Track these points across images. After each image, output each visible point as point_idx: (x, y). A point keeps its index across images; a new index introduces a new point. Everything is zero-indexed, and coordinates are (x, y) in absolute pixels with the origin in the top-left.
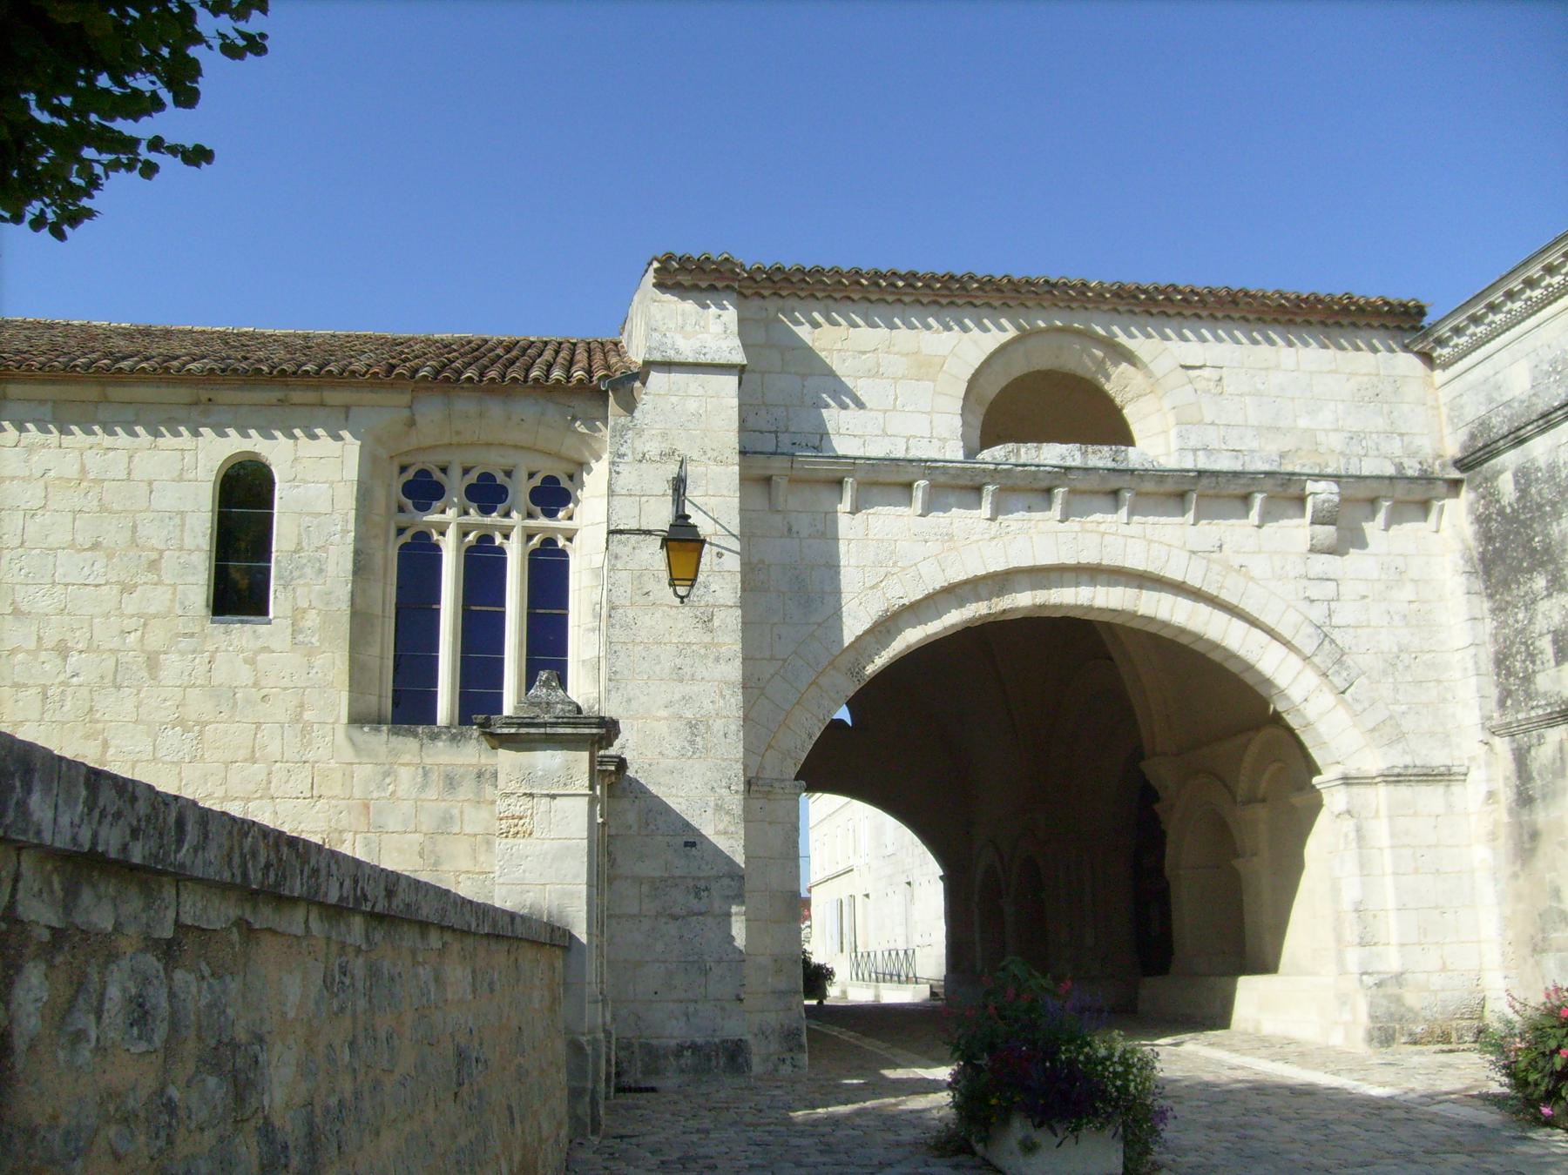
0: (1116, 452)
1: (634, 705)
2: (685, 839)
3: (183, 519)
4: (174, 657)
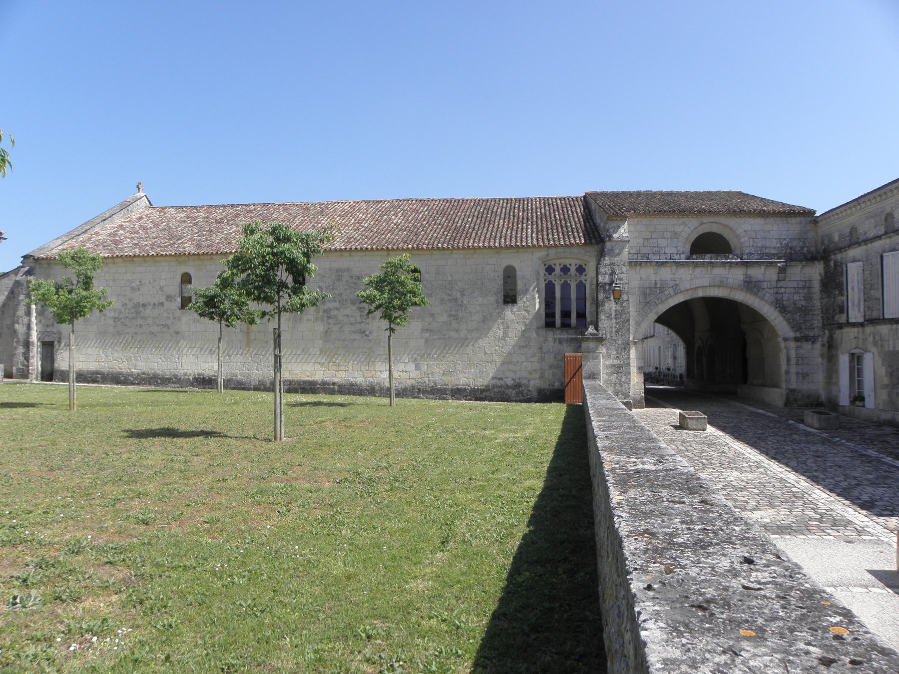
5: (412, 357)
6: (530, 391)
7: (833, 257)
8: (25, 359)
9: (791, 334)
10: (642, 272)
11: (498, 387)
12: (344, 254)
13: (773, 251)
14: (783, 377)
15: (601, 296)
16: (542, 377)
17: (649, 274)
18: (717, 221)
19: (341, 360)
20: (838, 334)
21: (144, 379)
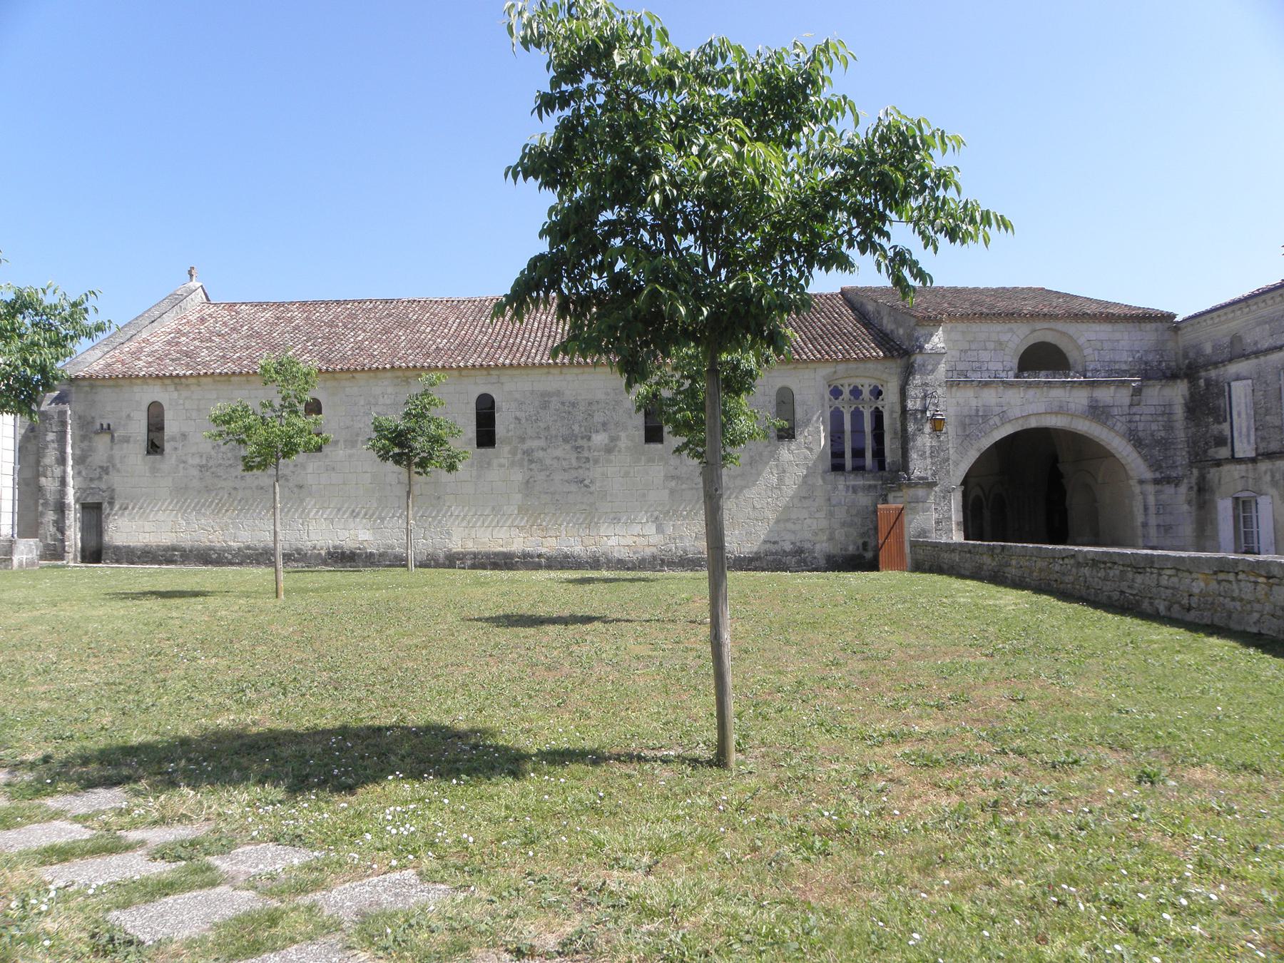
5: (652, 515)
6: (815, 558)
7: (1203, 374)
8: (58, 530)
9: (1149, 475)
10: (958, 394)
11: (772, 554)
12: (552, 371)
13: (1124, 367)
14: (1140, 531)
15: (911, 428)
16: (831, 539)
17: (969, 398)
19: (550, 521)
20: (1213, 473)
21: (249, 557)
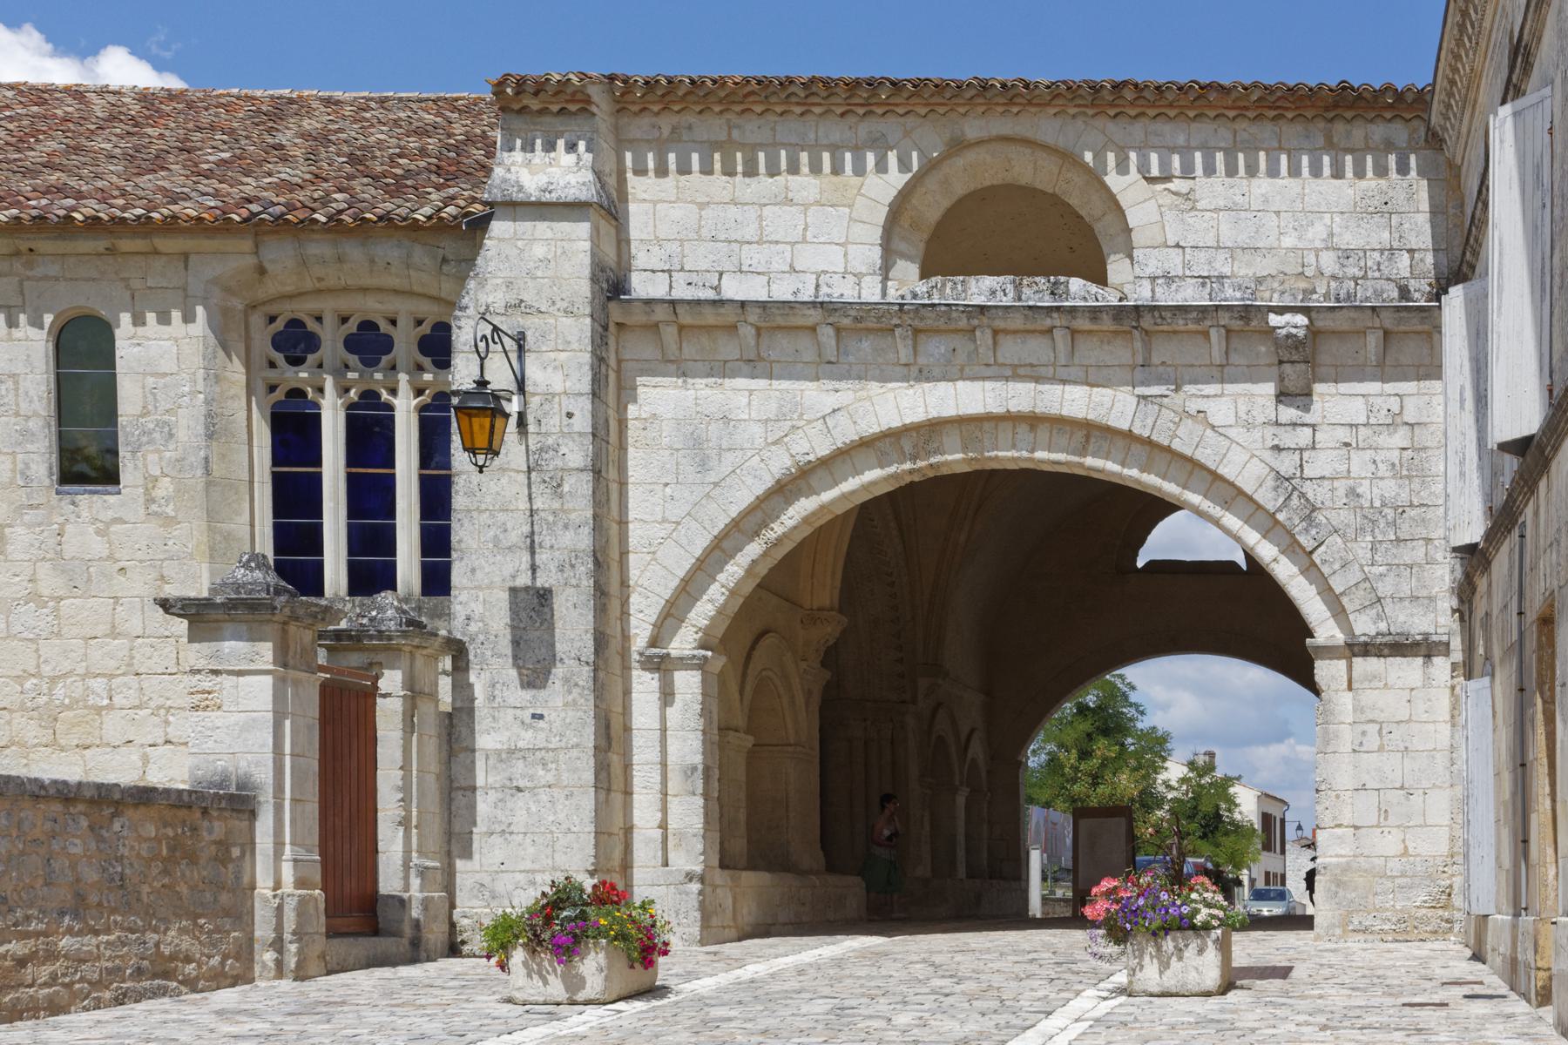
0: (1055, 284)
1: (479, 574)
2: (532, 711)
3: (16, 383)
4: (20, 530)
18: (1030, 134)
